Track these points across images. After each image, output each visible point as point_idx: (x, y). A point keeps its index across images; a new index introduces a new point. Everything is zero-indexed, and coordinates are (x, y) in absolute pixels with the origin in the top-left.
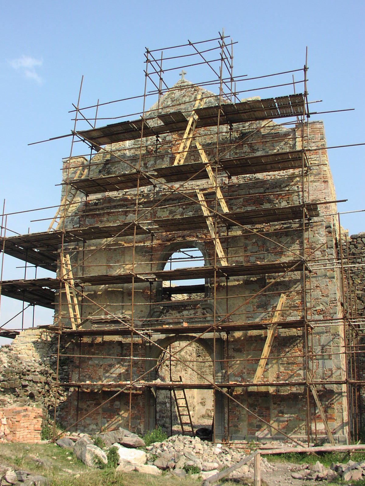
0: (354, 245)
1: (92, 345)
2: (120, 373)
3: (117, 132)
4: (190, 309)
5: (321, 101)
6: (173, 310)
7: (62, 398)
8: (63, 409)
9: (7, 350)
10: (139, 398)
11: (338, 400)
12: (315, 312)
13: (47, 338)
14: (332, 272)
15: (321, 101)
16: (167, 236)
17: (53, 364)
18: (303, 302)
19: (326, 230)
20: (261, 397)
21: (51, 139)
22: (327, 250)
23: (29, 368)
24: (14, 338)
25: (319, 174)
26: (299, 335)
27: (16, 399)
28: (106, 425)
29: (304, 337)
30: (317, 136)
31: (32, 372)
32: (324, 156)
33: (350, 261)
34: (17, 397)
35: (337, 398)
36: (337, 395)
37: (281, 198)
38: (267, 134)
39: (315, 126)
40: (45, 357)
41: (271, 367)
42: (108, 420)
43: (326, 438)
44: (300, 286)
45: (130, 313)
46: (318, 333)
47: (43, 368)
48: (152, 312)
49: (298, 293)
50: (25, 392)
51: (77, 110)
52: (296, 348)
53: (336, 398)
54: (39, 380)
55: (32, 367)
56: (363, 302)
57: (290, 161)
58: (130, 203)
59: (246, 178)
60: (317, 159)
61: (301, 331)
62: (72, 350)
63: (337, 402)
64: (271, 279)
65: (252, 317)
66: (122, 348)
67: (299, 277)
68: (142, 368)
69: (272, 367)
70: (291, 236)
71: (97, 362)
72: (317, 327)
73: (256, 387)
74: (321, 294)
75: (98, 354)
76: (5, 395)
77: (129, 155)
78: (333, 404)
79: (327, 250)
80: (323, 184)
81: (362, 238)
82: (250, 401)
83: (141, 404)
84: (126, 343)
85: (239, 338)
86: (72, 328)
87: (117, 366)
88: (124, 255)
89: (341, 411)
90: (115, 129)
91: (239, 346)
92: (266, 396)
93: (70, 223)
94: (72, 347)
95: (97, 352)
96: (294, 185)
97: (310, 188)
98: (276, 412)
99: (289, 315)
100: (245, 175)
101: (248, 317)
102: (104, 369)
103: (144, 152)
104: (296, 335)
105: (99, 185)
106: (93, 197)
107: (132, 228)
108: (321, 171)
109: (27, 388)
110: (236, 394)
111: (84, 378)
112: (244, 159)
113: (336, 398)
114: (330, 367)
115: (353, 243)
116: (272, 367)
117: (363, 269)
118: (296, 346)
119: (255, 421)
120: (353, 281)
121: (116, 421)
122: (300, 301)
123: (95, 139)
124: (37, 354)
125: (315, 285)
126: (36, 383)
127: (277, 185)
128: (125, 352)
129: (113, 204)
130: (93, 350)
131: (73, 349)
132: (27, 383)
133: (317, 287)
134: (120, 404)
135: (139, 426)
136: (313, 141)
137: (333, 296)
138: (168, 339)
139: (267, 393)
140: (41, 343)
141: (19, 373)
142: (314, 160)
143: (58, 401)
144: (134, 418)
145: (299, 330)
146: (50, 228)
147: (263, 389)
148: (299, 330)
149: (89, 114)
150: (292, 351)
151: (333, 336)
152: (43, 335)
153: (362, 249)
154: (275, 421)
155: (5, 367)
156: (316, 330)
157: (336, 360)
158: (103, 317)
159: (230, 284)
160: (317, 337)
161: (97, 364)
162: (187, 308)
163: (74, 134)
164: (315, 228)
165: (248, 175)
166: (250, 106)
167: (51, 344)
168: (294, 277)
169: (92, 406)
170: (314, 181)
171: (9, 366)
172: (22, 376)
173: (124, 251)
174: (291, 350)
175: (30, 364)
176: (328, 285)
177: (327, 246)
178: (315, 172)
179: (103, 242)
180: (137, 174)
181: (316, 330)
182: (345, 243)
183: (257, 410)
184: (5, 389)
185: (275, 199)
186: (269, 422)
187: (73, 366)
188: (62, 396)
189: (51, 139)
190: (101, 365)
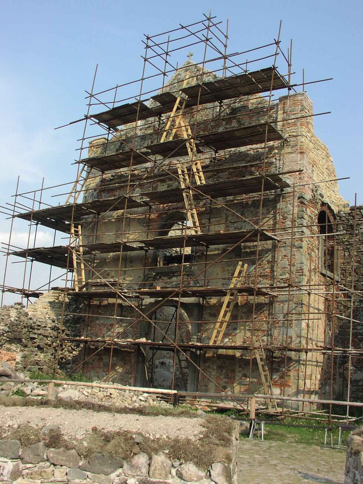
0: (353, 216)
1: (99, 306)
4: (177, 276)
6: (164, 276)
7: (74, 352)
11: (295, 367)
13: (64, 299)
14: (300, 242)
17: (65, 323)
18: (272, 271)
19: (299, 200)
20: (228, 359)
21: (71, 123)
22: (297, 220)
23: (39, 324)
25: (296, 145)
26: (266, 302)
27: (23, 348)
28: (105, 378)
29: (271, 303)
30: (297, 108)
31: (43, 327)
32: (302, 127)
33: (348, 233)
34: (24, 347)
35: (294, 366)
36: (294, 362)
39: (296, 98)
41: (239, 332)
42: (107, 373)
44: (271, 255)
46: (282, 302)
47: (56, 324)
49: (268, 262)
50: (33, 343)
51: (92, 96)
52: (263, 315)
53: (293, 365)
56: (357, 274)
58: (136, 178)
59: (231, 152)
60: (295, 131)
62: (84, 311)
63: (294, 369)
65: (227, 284)
66: (122, 310)
68: (136, 328)
69: (240, 332)
71: (102, 322)
72: (282, 294)
73: (225, 350)
76: (11, 344)
78: (290, 370)
79: (297, 220)
80: (299, 155)
81: (360, 209)
82: (219, 363)
83: (133, 360)
85: (215, 304)
86: (75, 290)
87: (117, 326)
89: (297, 378)
92: (232, 360)
93: (90, 197)
95: (103, 313)
97: (287, 160)
98: (240, 375)
100: (231, 149)
101: (223, 284)
103: (152, 131)
104: (264, 302)
105: (107, 163)
106: (108, 175)
107: (123, 202)
108: (297, 143)
109: (35, 341)
110: (208, 355)
112: (217, 134)
113: (293, 365)
114: (290, 335)
115: (351, 214)
116: (240, 332)
117: (359, 241)
119: (221, 382)
122: (270, 269)
123: (107, 121)
125: (284, 254)
126: (47, 337)
127: (258, 157)
128: (124, 313)
130: (100, 311)
131: (85, 309)
132: (36, 336)
133: (285, 256)
134: (117, 360)
136: (293, 113)
137: (299, 265)
138: (157, 302)
139: (234, 357)
140: (57, 303)
142: (292, 132)
145: (266, 298)
146: (66, 203)
147: (230, 352)
148: (266, 298)
149: (103, 98)
150: (259, 318)
151: (295, 305)
153: (359, 220)
155: (11, 320)
156: (281, 298)
158: (99, 280)
160: (281, 305)
161: (102, 324)
162: (175, 274)
163: (87, 118)
165: (233, 149)
166: (229, 83)
168: (266, 247)
169: (96, 360)
170: (291, 153)
173: (129, 221)
174: (258, 316)
175: (41, 320)
176: (296, 254)
178: (292, 143)
179: (114, 215)
181: (281, 298)
182: (344, 215)
183: (224, 372)
184: (10, 339)
185: (256, 171)
186: (233, 384)
188: (75, 351)
189: (71, 123)
190: (105, 325)
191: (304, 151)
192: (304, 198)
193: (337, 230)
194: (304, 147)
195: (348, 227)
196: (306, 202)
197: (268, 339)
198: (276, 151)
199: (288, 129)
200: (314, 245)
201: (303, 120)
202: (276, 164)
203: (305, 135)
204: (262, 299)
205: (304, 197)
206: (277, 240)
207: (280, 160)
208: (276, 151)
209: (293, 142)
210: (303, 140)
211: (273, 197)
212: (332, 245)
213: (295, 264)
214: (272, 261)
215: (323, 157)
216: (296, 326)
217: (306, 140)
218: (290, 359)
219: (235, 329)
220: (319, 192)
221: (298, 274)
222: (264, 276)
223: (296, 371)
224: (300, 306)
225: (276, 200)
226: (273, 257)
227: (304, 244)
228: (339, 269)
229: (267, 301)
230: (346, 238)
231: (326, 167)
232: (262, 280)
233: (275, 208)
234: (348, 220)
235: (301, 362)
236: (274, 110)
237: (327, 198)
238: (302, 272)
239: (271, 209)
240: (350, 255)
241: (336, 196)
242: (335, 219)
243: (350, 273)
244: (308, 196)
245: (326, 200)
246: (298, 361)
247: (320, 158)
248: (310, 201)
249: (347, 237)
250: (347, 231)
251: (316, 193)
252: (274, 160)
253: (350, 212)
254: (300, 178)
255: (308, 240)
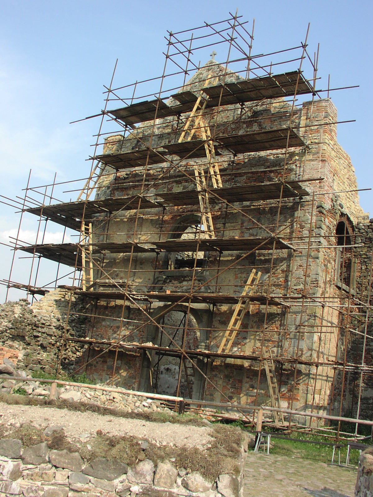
1: (106, 308)
2: (124, 334)
3: (141, 112)
5: (320, 78)
7: (78, 353)
8: (78, 363)
9: (24, 303)
10: (137, 359)
11: (304, 380)
12: (295, 291)
13: (71, 298)
14: (316, 252)
15: (320, 78)
16: (178, 210)
18: (286, 281)
19: (317, 210)
20: (236, 369)
21: (87, 118)
24: (44, 295)
25: (318, 153)
26: (278, 312)
27: (25, 346)
29: (283, 314)
30: (321, 114)
32: (325, 135)
34: (26, 345)
35: (303, 379)
36: (304, 376)
37: (281, 177)
38: (277, 113)
39: (320, 105)
40: (66, 315)
43: (287, 417)
44: (286, 264)
45: (140, 281)
47: (60, 323)
48: (156, 281)
49: (283, 271)
50: (36, 342)
51: (110, 91)
53: (303, 378)
54: (52, 333)
55: (48, 321)
57: (283, 139)
58: (151, 178)
59: (251, 156)
61: (280, 309)
62: (90, 311)
64: (261, 256)
65: (239, 292)
66: (129, 312)
67: (285, 256)
68: (143, 332)
70: (284, 214)
71: (108, 323)
73: (233, 359)
74: (303, 274)
75: (110, 316)
76: (14, 341)
77: (157, 133)
78: (299, 384)
79: (315, 230)
80: (320, 163)
83: (138, 365)
84: (133, 308)
85: (225, 312)
88: (142, 227)
89: (306, 392)
90: (138, 108)
91: (224, 319)
92: (241, 369)
94: (90, 309)
96: (292, 163)
98: (248, 385)
99: (271, 293)
100: (250, 153)
101: (235, 292)
102: (113, 330)
104: (276, 312)
106: (123, 173)
108: (319, 150)
109: (39, 339)
111: (97, 337)
113: (303, 378)
115: (370, 227)
116: (250, 341)
118: (274, 324)
119: (227, 392)
120: (367, 266)
121: (116, 378)
123: (125, 117)
124: (57, 310)
125: (299, 264)
126: (51, 336)
127: (278, 163)
129: (137, 179)
130: (107, 312)
131: (92, 310)
132: (40, 334)
133: (300, 266)
135: (133, 386)
136: (316, 119)
137: (314, 276)
139: (241, 367)
140: (63, 302)
141: (31, 325)
142: (315, 139)
143: (75, 356)
144: (132, 377)
145: (279, 308)
146: (78, 199)
147: (239, 362)
148: (279, 308)
149: (121, 94)
150: (270, 328)
151: (308, 317)
152: (67, 296)
154: (245, 395)
156: (293, 309)
157: (308, 341)
159: (221, 259)
160: (294, 316)
162: (186, 279)
163: (104, 113)
164: (306, 208)
165: (252, 153)
167: (75, 304)
170: (312, 160)
171: (21, 317)
172: (34, 328)
174: (269, 326)
175: (45, 318)
176: (311, 265)
177: (316, 225)
178: (313, 150)
179: (126, 214)
180: (147, 150)
181: (293, 309)
182: (363, 227)
183: (231, 382)
185: (275, 177)
186: (240, 394)
187: (90, 325)
188: (79, 351)
189: (87, 118)
191: (326, 159)
192: (323, 208)
193: (355, 242)
194: (326, 155)
195: (367, 240)
196: (325, 212)
197: (278, 351)
198: (297, 158)
199: (310, 136)
200: (330, 256)
201: (326, 127)
202: (296, 171)
203: (328, 142)
204: (274, 309)
205: (323, 206)
206: (294, 249)
207: (300, 167)
208: (297, 158)
209: (314, 149)
210: (325, 148)
211: (291, 204)
212: (349, 257)
213: (310, 275)
214: (286, 271)
215: (345, 166)
216: (308, 339)
217: (329, 147)
218: (299, 372)
219: (245, 338)
220: (338, 202)
221: (313, 285)
222: (278, 286)
223: (305, 384)
224: (313, 318)
225: (294, 208)
226: (288, 266)
227: (321, 255)
228: (355, 282)
229: (279, 311)
230: (364, 251)
231: (347, 176)
232: (275, 289)
233: (292, 216)
234: (367, 233)
235: (311, 376)
236: (296, 116)
237: (347, 208)
238: (317, 284)
239: (288, 216)
240: (367, 268)
241: (356, 207)
242: (353, 230)
243: (366, 287)
244: (328, 205)
245: (346, 211)
246: (308, 375)
247: (342, 167)
248: (329, 211)
249: (365, 250)
250: (365, 244)
251: (335, 203)
252: (294, 167)
253: (369, 224)
254: (320, 187)
255: (324, 251)
